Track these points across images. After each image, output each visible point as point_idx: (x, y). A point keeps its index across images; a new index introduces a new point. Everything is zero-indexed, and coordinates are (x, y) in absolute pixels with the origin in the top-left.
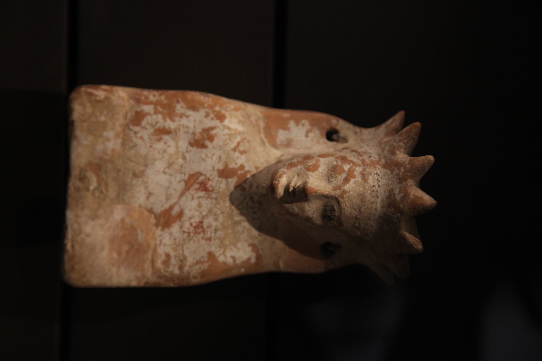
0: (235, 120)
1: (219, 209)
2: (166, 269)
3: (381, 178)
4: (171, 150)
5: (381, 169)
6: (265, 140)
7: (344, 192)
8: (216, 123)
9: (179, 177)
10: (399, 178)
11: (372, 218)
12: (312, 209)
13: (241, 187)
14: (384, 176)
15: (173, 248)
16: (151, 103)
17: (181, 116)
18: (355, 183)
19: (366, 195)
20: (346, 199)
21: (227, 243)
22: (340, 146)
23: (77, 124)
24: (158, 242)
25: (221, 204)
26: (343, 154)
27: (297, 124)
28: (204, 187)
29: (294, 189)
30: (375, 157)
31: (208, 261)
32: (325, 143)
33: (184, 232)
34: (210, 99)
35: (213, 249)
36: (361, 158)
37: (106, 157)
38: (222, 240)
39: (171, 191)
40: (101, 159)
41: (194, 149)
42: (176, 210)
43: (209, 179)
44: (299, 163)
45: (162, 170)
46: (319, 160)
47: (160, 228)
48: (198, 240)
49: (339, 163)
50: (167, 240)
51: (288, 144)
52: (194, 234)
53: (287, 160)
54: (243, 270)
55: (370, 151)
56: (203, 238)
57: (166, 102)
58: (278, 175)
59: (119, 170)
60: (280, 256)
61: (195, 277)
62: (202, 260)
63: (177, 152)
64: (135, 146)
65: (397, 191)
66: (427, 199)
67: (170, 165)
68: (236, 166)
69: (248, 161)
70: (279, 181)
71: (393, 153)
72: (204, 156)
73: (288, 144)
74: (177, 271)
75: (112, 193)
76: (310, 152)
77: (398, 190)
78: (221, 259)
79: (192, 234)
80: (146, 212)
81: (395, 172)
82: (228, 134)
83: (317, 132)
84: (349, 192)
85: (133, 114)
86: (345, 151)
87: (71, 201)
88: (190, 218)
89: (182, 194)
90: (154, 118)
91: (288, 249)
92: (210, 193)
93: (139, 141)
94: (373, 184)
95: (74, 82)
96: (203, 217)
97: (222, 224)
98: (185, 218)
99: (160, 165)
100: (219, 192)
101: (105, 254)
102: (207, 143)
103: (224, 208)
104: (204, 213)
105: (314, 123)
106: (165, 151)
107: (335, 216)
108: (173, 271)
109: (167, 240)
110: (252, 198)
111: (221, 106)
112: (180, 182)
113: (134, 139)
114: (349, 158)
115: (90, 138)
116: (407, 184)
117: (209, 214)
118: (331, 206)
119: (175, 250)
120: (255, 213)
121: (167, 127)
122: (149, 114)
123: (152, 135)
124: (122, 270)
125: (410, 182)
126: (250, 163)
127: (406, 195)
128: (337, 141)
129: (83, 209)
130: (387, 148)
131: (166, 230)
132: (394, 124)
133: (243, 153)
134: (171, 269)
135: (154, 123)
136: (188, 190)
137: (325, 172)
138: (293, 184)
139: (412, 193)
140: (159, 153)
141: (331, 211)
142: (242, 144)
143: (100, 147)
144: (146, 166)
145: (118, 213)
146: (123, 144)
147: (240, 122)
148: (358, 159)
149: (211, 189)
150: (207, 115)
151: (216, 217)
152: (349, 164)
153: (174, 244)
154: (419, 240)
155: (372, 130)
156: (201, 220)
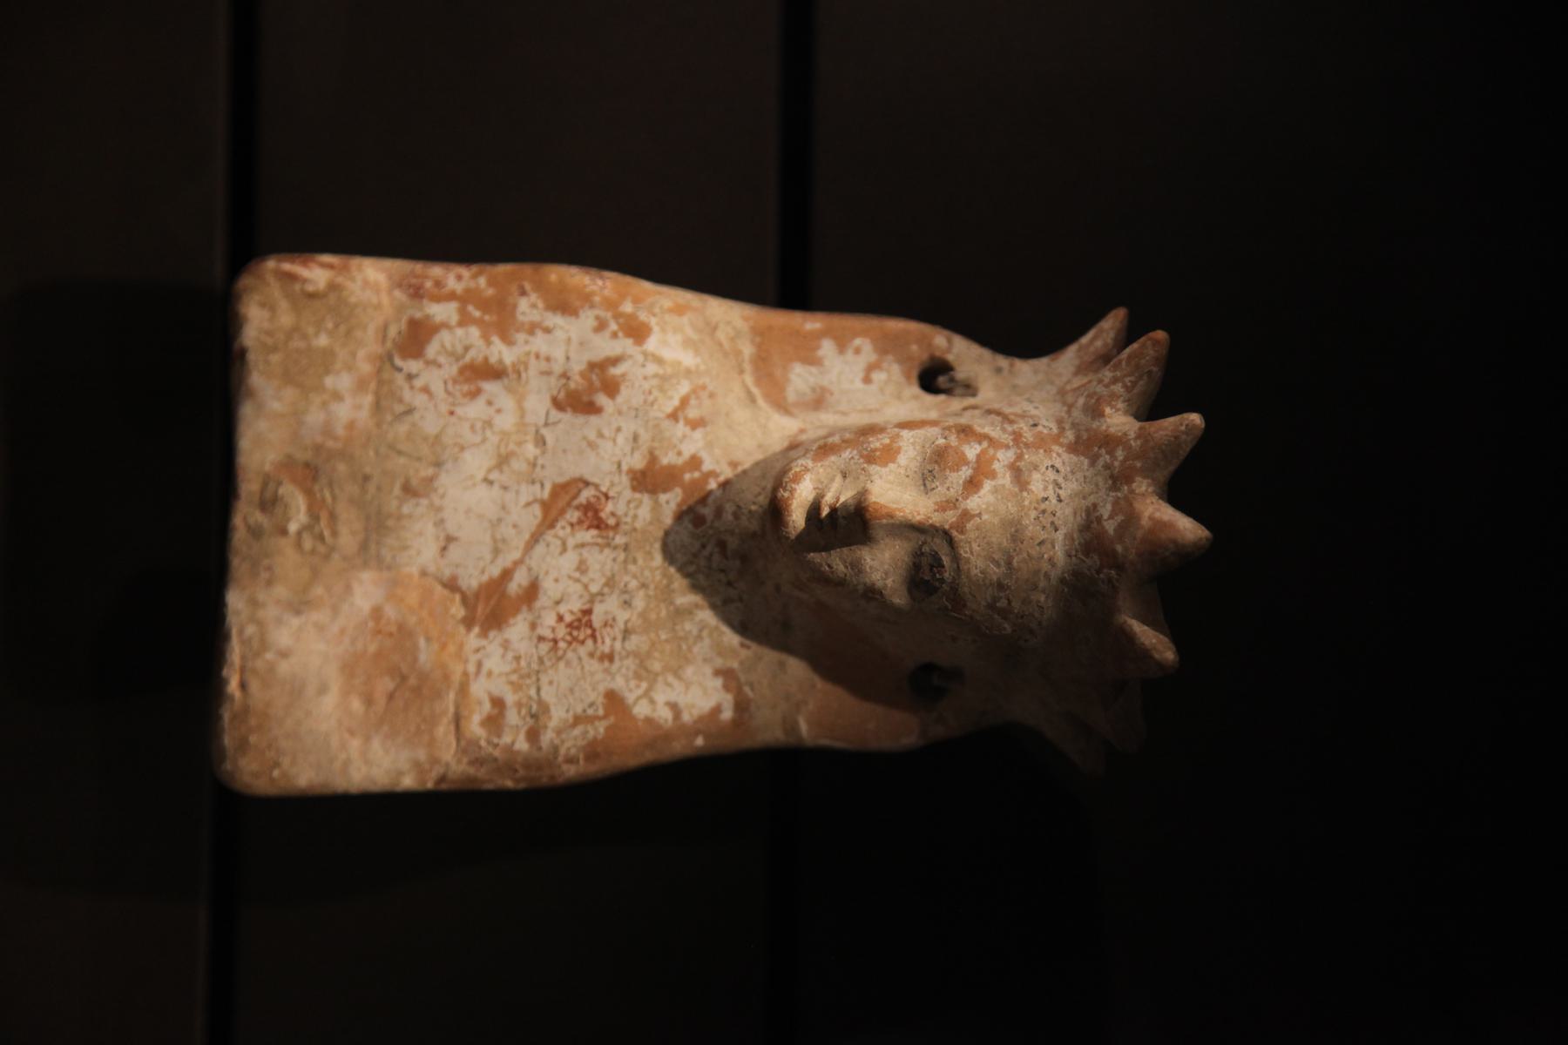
0: (674, 339)
1: (635, 577)
2: (496, 740)
3: (1065, 478)
4: (506, 421)
5: (1066, 456)
6: (755, 391)
7: (966, 515)
8: (624, 345)
9: (527, 492)
10: (1112, 476)
11: (1042, 584)
12: (882, 564)
13: (690, 515)
14: (1073, 472)
15: (512, 683)
16: (452, 296)
17: (532, 329)
18: (995, 490)
19: (1026, 522)
20: (972, 535)
21: (656, 666)
22: (956, 404)
23: (252, 357)
24: (472, 668)
25: (640, 562)
26: (963, 421)
27: (842, 347)
28: (593, 517)
29: (834, 510)
30: (1048, 426)
31: (605, 717)
32: (916, 397)
33: (541, 639)
34: (608, 283)
35: (619, 683)
36: (1009, 428)
37: (330, 444)
38: (642, 659)
39: (506, 531)
40: (318, 448)
41: (567, 417)
42: (520, 580)
43: (607, 497)
44: (846, 443)
45: (480, 475)
46: (898, 435)
47: (476, 630)
48: (580, 659)
49: (953, 440)
50: (496, 661)
51: (819, 400)
52: (570, 643)
53: (815, 441)
54: (700, 741)
55: (1034, 412)
56: (591, 655)
57: (490, 292)
58: (791, 475)
59: (366, 478)
60: (797, 702)
61: (571, 760)
62: (590, 712)
63: (522, 425)
64: (410, 411)
65: (1105, 511)
66: (1187, 528)
67: (503, 461)
68: (680, 461)
69: (709, 445)
70: (792, 491)
71: (1095, 411)
72: (592, 436)
73: (819, 400)
74: (522, 745)
75: (348, 540)
76: (877, 419)
77: (1109, 507)
78: (641, 710)
79: (562, 645)
80: (439, 589)
81: (1101, 462)
82: (656, 376)
83: (896, 370)
84: (979, 515)
85: (403, 325)
86: (969, 413)
87: (239, 566)
88: (558, 603)
89: (535, 538)
90: (457, 336)
91: (819, 683)
92: (611, 534)
93: (420, 400)
94: (1044, 495)
95: (245, 251)
96: (593, 599)
97: (643, 615)
98: (543, 601)
99: (476, 462)
100: (635, 530)
101: (330, 702)
102: (602, 399)
103: (647, 573)
104: (594, 588)
105: (886, 347)
106: (488, 424)
107: (942, 581)
108: (513, 743)
109: (496, 661)
110: (722, 545)
111: (637, 301)
112: (528, 504)
113: (407, 395)
114: (978, 429)
115: (290, 393)
116: (1132, 491)
117: (606, 590)
118: (931, 554)
119: (516, 687)
120: (729, 584)
121: (493, 360)
122: (445, 325)
123: (455, 382)
124: (376, 744)
125: (1142, 485)
126: (717, 451)
127: (1131, 518)
128: (948, 392)
129: (269, 583)
130: (1081, 401)
131: (492, 634)
132: (1099, 343)
133: (695, 424)
134: (507, 739)
135: (459, 349)
136: (552, 526)
137: (914, 466)
138: (829, 498)
139: (1147, 514)
140: (472, 427)
141: (932, 567)
142: (693, 402)
143: (315, 417)
144: (438, 464)
145: (366, 592)
146: (378, 407)
147: (687, 343)
148: (1004, 430)
149: (611, 522)
150: (601, 326)
151: (626, 597)
152: (980, 443)
153: (515, 671)
154: (1166, 639)
155: (1042, 363)
156: (586, 607)
